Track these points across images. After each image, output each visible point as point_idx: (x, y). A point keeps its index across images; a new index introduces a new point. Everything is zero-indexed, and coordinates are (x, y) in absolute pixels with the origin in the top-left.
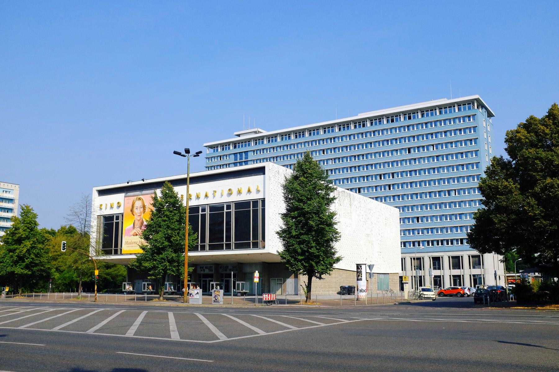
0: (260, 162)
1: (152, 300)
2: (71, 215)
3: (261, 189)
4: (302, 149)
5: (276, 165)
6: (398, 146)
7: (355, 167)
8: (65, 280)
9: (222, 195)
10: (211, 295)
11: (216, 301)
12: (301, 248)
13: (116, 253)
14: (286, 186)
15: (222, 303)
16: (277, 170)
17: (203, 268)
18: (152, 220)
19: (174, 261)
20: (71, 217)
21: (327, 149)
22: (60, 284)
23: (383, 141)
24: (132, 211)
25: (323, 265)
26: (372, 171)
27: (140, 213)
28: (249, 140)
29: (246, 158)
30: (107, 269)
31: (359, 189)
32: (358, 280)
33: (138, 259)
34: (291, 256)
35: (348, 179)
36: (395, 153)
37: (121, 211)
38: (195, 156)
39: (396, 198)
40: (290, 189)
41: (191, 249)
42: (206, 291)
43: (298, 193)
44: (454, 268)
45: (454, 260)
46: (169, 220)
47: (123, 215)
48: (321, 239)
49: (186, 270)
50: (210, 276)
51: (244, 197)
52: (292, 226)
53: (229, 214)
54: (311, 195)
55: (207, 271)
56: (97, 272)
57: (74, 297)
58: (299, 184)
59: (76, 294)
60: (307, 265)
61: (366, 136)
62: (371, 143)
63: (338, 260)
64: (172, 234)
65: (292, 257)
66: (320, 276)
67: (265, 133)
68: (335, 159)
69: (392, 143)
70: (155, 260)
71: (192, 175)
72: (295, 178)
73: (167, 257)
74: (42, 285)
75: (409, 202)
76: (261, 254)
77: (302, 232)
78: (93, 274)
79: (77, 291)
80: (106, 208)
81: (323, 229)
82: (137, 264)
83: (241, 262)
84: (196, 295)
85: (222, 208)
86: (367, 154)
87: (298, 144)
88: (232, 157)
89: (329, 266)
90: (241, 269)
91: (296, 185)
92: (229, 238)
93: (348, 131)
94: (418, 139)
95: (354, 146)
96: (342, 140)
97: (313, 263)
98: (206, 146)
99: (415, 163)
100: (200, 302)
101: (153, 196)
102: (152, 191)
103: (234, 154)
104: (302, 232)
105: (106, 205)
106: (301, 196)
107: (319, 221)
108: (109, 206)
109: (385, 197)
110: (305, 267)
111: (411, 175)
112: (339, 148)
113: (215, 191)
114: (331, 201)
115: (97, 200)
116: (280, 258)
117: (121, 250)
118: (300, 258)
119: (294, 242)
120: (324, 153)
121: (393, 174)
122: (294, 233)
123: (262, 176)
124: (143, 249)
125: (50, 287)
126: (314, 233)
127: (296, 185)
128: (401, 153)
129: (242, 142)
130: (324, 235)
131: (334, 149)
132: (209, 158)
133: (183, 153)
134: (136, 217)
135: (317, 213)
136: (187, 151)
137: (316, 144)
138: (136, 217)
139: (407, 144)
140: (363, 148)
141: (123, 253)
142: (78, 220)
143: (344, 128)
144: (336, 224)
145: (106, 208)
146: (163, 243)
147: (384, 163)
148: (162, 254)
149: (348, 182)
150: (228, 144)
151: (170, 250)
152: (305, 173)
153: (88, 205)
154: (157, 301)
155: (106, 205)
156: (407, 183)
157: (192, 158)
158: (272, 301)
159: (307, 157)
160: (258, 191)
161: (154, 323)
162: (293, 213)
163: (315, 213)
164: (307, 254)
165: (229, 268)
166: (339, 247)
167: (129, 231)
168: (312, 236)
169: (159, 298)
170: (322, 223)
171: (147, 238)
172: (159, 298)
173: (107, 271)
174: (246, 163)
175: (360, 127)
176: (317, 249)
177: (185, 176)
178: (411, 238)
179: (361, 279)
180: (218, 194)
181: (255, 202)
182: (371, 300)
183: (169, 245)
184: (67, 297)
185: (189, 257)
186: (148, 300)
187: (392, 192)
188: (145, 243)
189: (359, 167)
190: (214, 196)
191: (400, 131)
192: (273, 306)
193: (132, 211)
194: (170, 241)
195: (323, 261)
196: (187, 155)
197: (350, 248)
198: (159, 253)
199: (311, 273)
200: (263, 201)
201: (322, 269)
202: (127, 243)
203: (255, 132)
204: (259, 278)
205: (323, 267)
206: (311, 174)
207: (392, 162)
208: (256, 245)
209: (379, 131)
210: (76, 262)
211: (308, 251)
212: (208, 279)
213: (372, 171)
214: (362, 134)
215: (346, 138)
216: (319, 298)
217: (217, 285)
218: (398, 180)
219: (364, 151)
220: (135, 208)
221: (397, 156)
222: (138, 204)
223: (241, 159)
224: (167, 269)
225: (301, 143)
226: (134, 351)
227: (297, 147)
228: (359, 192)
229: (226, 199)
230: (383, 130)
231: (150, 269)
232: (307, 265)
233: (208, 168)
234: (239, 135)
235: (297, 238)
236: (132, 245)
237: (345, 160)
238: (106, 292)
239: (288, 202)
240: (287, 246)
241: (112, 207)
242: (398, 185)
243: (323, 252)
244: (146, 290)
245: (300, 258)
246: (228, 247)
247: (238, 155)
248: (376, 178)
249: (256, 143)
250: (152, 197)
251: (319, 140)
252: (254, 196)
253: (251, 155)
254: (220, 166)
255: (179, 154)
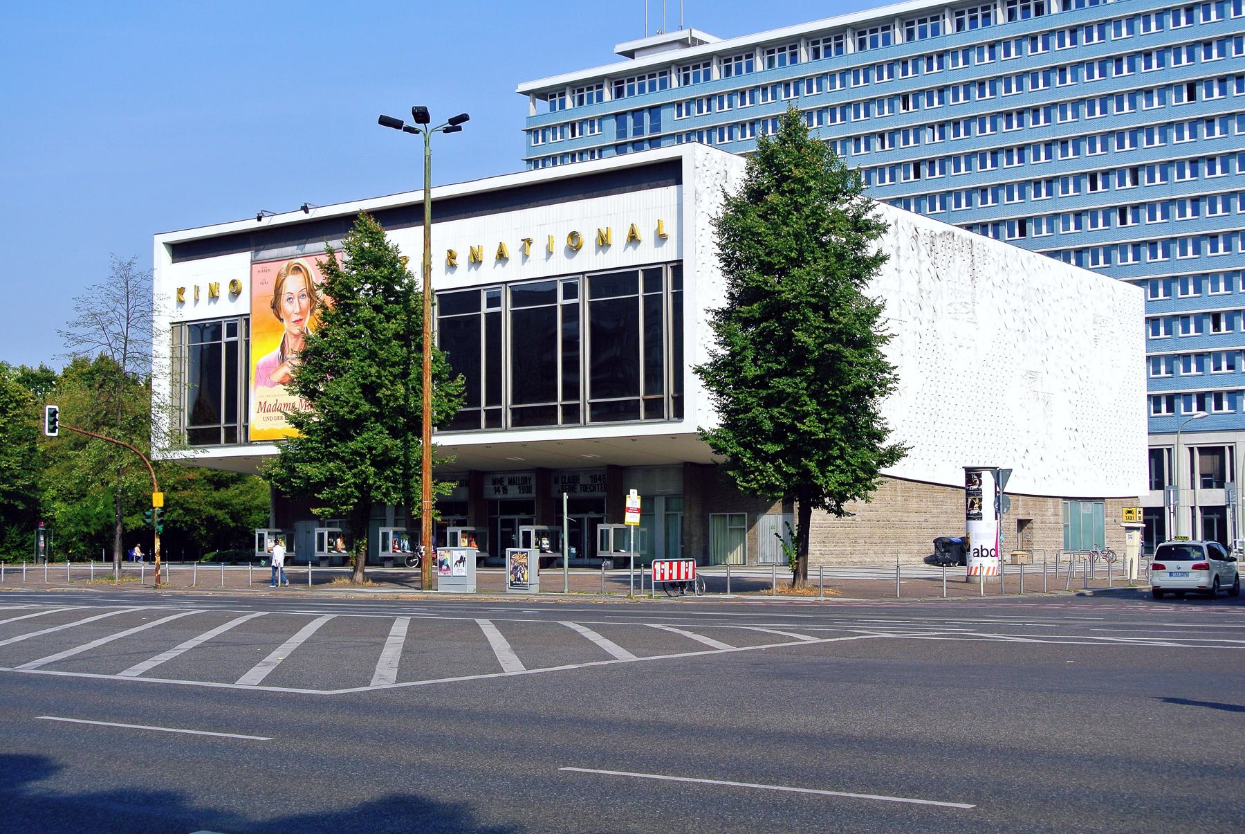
0: (592, 157)
1: (330, 581)
2: (77, 324)
3: (670, 230)
4: (775, 106)
5: (717, 154)
6: (1152, 75)
7: (1009, 151)
8: (87, 525)
9: (549, 253)
10: (504, 566)
11: (517, 582)
12: (772, 418)
13: (232, 439)
14: (724, 222)
15: (535, 589)
16: (720, 168)
17: (501, 481)
18: (323, 334)
19: (393, 462)
20: (80, 331)
21: (917, 94)
22: (71, 536)
23: (1103, 62)
24: (275, 306)
25: (842, 471)
26: (1066, 164)
27: (302, 312)
28: (663, 69)
29: (656, 127)
30: (217, 489)
31: (1023, 223)
32: (969, 517)
33: (284, 457)
34: (740, 444)
35: (984, 190)
36: (1142, 101)
37: (242, 306)
38: (447, 130)
39: (1146, 252)
40: (739, 233)
41: (438, 422)
42: (492, 555)
43: (759, 242)
44: (1207, 484)
45: (1208, 458)
46: (377, 337)
47: (247, 321)
48: (834, 387)
49: (427, 493)
50: (492, 507)
51: (618, 258)
52: (744, 348)
53: (571, 313)
54: (801, 252)
55: (514, 493)
56: (158, 500)
57: (99, 574)
58: (764, 217)
59: (107, 566)
60: (793, 470)
61: (1046, 46)
62: (1062, 70)
63: (894, 455)
64: (379, 377)
65: (746, 446)
66: (838, 505)
67: (715, 44)
68: (942, 125)
69: (1132, 68)
70: (335, 456)
71: (438, 193)
72: (755, 194)
73: (370, 449)
74: (18, 540)
75: (1186, 263)
76: (673, 437)
77: (775, 366)
78: (143, 504)
79: (110, 558)
80: (197, 300)
81: (838, 356)
82: (283, 472)
83: (620, 463)
84: (459, 562)
85: (552, 296)
86: (1048, 108)
87: (820, 78)
88: (611, 124)
89: (862, 475)
90: (600, 484)
91: (753, 220)
92: (572, 390)
93: (987, 30)
94: (1222, 53)
95: (1007, 79)
96: (966, 61)
97: (812, 466)
98: (526, 93)
99: (1211, 132)
100: (471, 588)
101: (325, 259)
102: (321, 246)
103: (616, 115)
104: (775, 366)
105: (197, 289)
106: (769, 254)
107: (826, 330)
108: (204, 295)
109: (1108, 250)
110: (787, 477)
111: (1194, 173)
112: (955, 88)
113: (528, 242)
114: (868, 267)
115: (170, 277)
116: (711, 450)
117: (246, 428)
118: (771, 448)
119: (750, 400)
120: (906, 107)
121: (1135, 171)
122: (751, 371)
123: (674, 189)
124: (299, 425)
125: (42, 545)
126: (812, 370)
127: (753, 220)
128: (1163, 101)
129: (641, 73)
130: (841, 379)
131: (941, 90)
132: (536, 131)
133: (410, 121)
134: (289, 327)
135: (822, 307)
136: (422, 115)
137: (880, 77)
138: (289, 327)
139: (1182, 70)
140: (1035, 85)
141: (251, 438)
142: (104, 340)
143: (973, 19)
144: (884, 340)
145: (197, 300)
146: (356, 406)
147: (1105, 136)
148: (352, 439)
149: (984, 201)
150: (597, 83)
151: (379, 426)
152: (785, 179)
153: (134, 292)
154: (345, 585)
155: (197, 289)
156: (1181, 203)
157: (440, 140)
158: (682, 585)
159: (791, 125)
160: (661, 238)
161: (234, 644)
162: (744, 308)
163: (815, 308)
164: (791, 437)
165: (582, 481)
166: (892, 411)
167: (268, 368)
168: (807, 378)
169: (351, 576)
170: (836, 337)
171: (310, 394)
172: (351, 576)
173: (215, 494)
174: (655, 143)
175: (1026, 15)
176: (821, 421)
177: (417, 196)
178: (1192, 381)
179: (979, 517)
180: (537, 251)
181: (653, 275)
182: (1001, 585)
183: (374, 414)
184: (76, 576)
185: (434, 446)
186: (315, 582)
187: (1133, 232)
188: (299, 402)
189: (1021, 149)
190: (526, 256)
191: (1160, 25)
192: (690, 597)
193: (275, 306)
194: (375, 401)
195: (841, 457)
196: (420, 126)
197: (930, 416)
198: (345, 437)
199: (806, 496)
200: (678, 267)
201: (842, 484)
202: (263, 407)
203: (683, 43)
204: (642, 511)
205: (843, 478)
206: (800, 181)
207: (1134, 132)
208: (655, 411)
209: (1089, 28)
210: (101, 466)
211: (793, 429)
212: (586, 517)
213: (1066, 164)
214: (1034, 38)
215: (981, 55)
216: (828, 574)
217: (540, 534)
218: (1153, 190)
219: (1039, 95)
220: (284, 298)
221: (1151, 112)
222: (294, 284)
223: (638, 130)
224: (370, 487)
225: (832, 75)
226: (913, 791)
227: (820, 88)
228: (1023, 232)
229: (561, 265)
230: (1102, 25)
231: (319, 487)
232: (793, 470)
233: (534, 163)
234: (630, 54)
235: (758, 387)
236: (271, 413)
237: (975, 127)
238: (216, 560)
239: (731, 272)
240: (732, 414)
241: (214, 297)
242: (1151, 207)
243: (843, 430)
244: (325, 553)
245: (771, 448)
246: (572, 416)
247: (630, 120)
248: (1077, 188)
249: (728, 69)
250: (320, 265)
251: (891, 64)
252: (647, 254)
253: (668, 115)
254: (592, 152)
255: (397, 124)
